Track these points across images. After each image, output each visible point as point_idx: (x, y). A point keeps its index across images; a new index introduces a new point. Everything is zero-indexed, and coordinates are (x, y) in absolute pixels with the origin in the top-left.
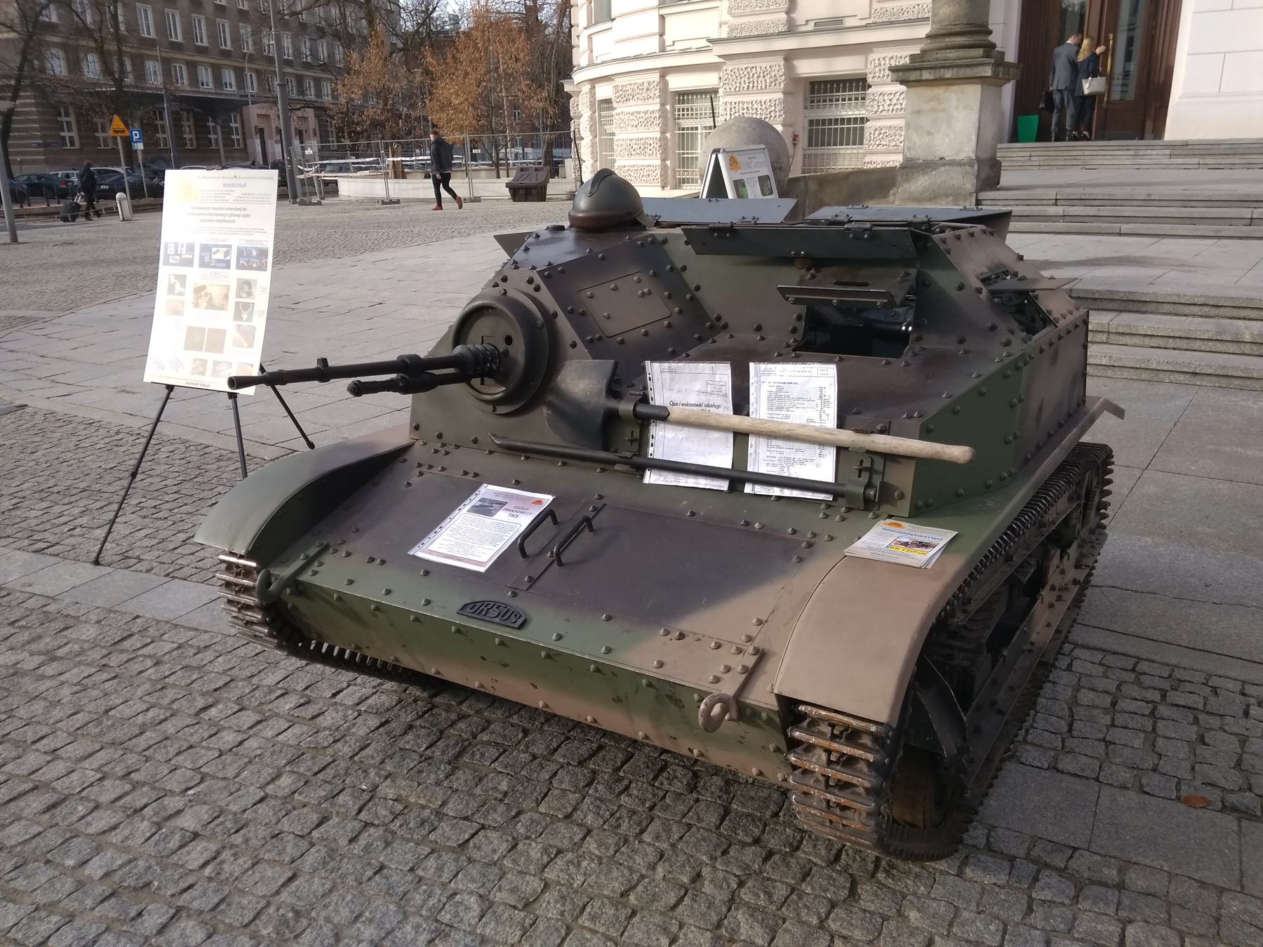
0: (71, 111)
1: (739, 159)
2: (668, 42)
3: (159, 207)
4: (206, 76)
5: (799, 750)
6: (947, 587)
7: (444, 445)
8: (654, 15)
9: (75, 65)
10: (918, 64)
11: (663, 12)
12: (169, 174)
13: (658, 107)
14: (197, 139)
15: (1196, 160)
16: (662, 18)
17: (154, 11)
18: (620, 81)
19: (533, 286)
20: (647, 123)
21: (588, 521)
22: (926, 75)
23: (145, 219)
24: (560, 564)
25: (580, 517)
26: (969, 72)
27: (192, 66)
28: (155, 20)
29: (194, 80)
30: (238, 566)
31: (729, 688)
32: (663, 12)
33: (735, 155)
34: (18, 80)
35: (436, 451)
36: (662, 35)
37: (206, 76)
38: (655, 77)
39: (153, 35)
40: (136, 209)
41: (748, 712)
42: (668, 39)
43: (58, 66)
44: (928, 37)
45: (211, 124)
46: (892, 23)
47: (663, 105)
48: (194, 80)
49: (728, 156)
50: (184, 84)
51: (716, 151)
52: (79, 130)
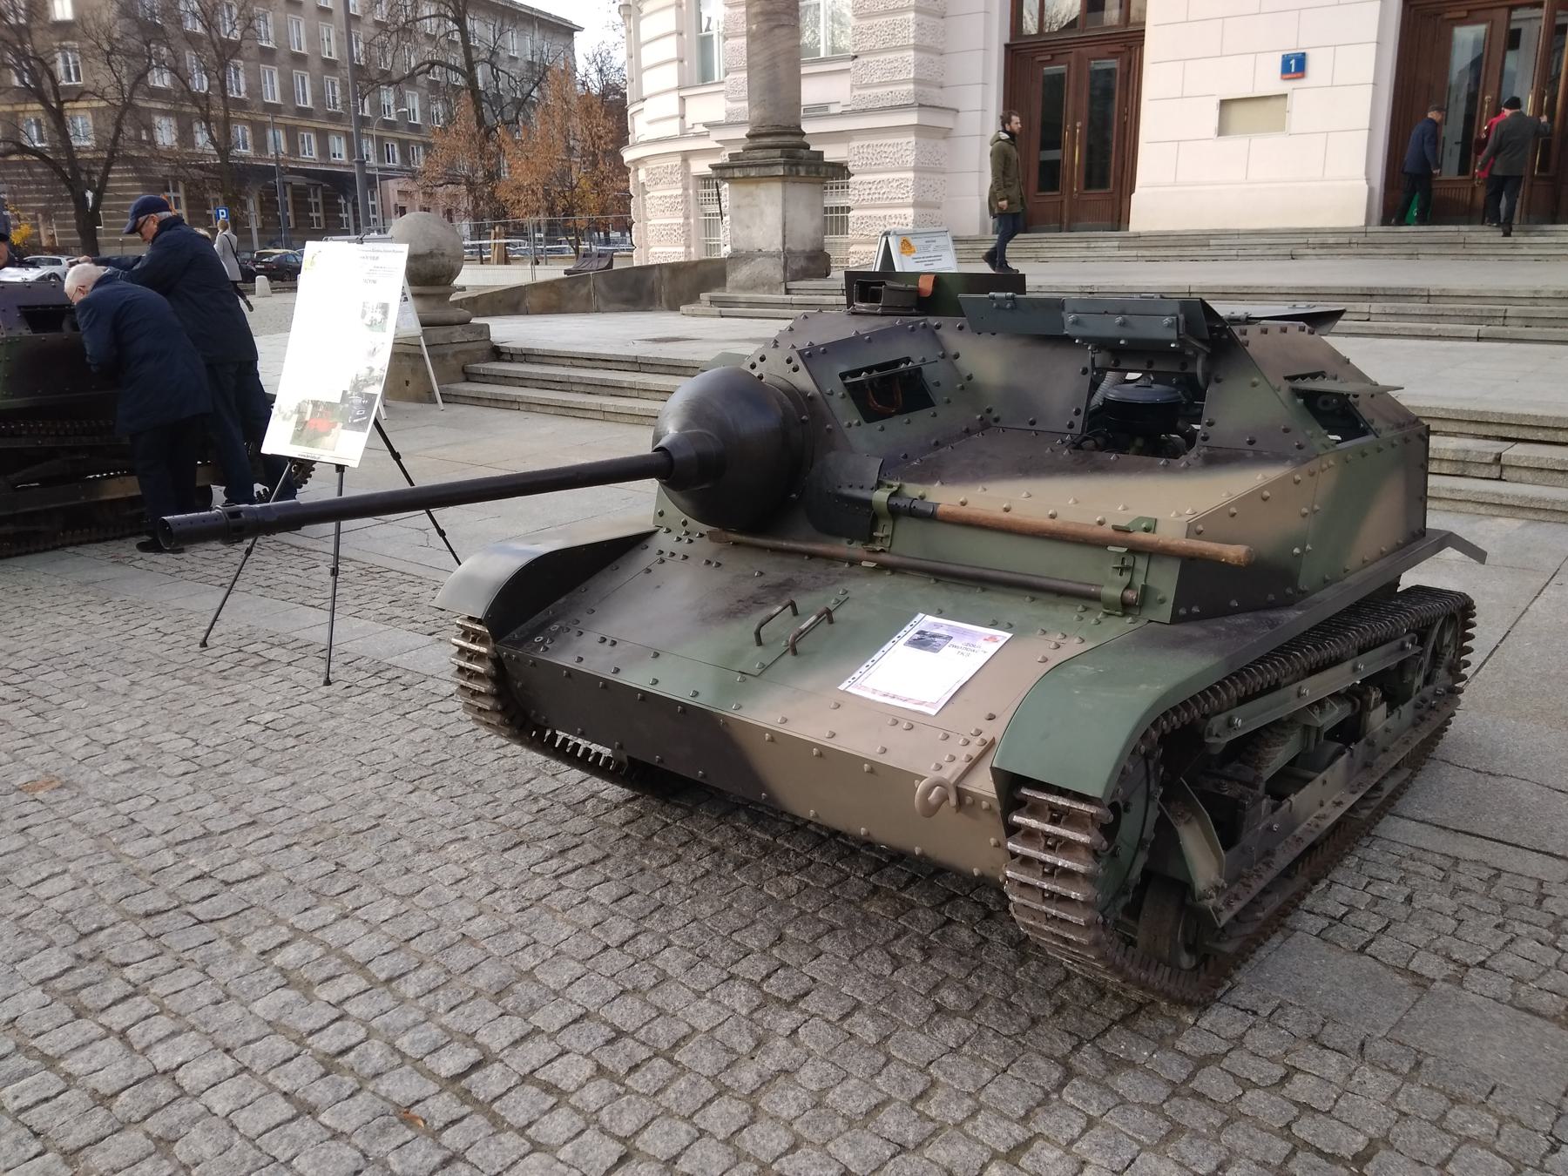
0: (181, 187)
1: (913, 242)
2: (689, 125)
3: (295, 289)
4: (338, 146)
5: (1017, 836)
6: (1190, 681)
7: (687, 533)
8: (674, 97)
9: (185, 135)
10: (736, 162)
11: (683, 93)
12: (311, 247)
13: (680, 192)
14: (326, 218)
15: (1134, 253)
16: (683, 99)
17: (280, 73)
18: (652, 164)
19: (791, 366)
20: (672, 208)
21: (829, 612)
22: (737, 173)
23: (280, 299)
24: (795, 652)
25: (821, 609)
26: (767, 171)
27: (322, 135)
28: (281, 83)
29: (324, 150)
30: (470, 651)
31: (950, 773)
32: (683, 93)
33: (909, 238)
34: (111, 154)
35: (679, 539)
36: (683, 117)
37: (338, 146)
38: (678, 161)
39: (278, 100)
40: (274, 290)
41: (969, 800)
42: (689, 122)
43: (166, 135)
44: (748, 136)
45: (342, 201)
46: (871, 110)
47: (686, 189)
48: (324, 150)
49: (900, 239)
50: (310, 154)
51: (887, 234)
52: (189, 207)
